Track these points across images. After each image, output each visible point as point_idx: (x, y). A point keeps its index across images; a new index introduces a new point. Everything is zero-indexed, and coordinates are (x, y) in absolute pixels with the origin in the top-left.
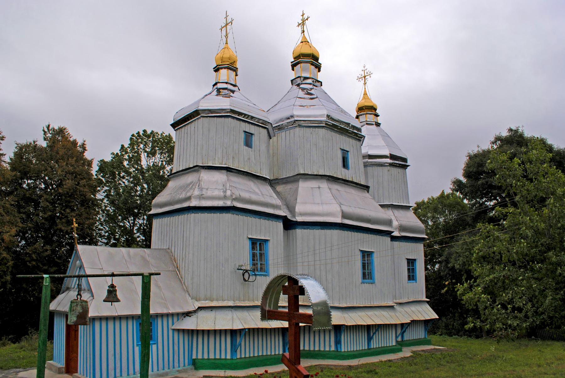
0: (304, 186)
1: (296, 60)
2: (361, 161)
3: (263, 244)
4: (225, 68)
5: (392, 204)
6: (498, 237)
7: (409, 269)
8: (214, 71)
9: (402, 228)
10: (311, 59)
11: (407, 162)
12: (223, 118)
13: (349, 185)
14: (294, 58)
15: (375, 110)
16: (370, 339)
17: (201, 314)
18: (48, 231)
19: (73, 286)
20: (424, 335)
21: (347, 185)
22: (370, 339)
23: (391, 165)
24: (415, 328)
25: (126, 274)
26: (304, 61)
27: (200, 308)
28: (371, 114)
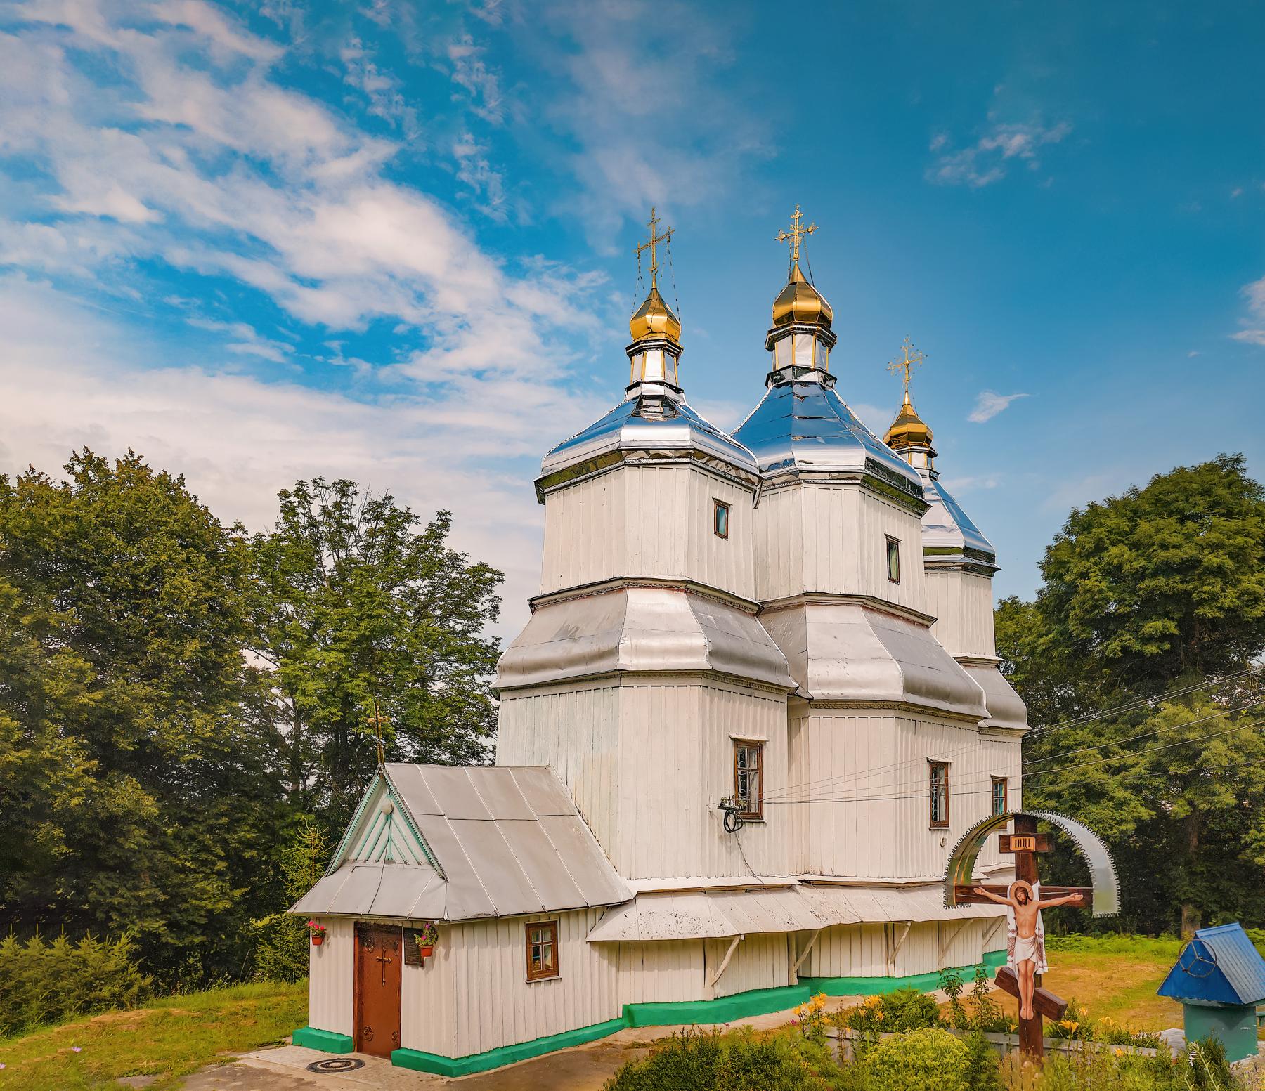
0: (815, 616)
1: (783, 327)
2: (920, 560)
4: (657, 348)
8: (628, 354)
15: (929, 441)
17: (640, 901)
19: (363, 856)
23: (966, 568)
25: (365, 827)
26: (802, 329)
27: (640, 894)
28: (921, 452)
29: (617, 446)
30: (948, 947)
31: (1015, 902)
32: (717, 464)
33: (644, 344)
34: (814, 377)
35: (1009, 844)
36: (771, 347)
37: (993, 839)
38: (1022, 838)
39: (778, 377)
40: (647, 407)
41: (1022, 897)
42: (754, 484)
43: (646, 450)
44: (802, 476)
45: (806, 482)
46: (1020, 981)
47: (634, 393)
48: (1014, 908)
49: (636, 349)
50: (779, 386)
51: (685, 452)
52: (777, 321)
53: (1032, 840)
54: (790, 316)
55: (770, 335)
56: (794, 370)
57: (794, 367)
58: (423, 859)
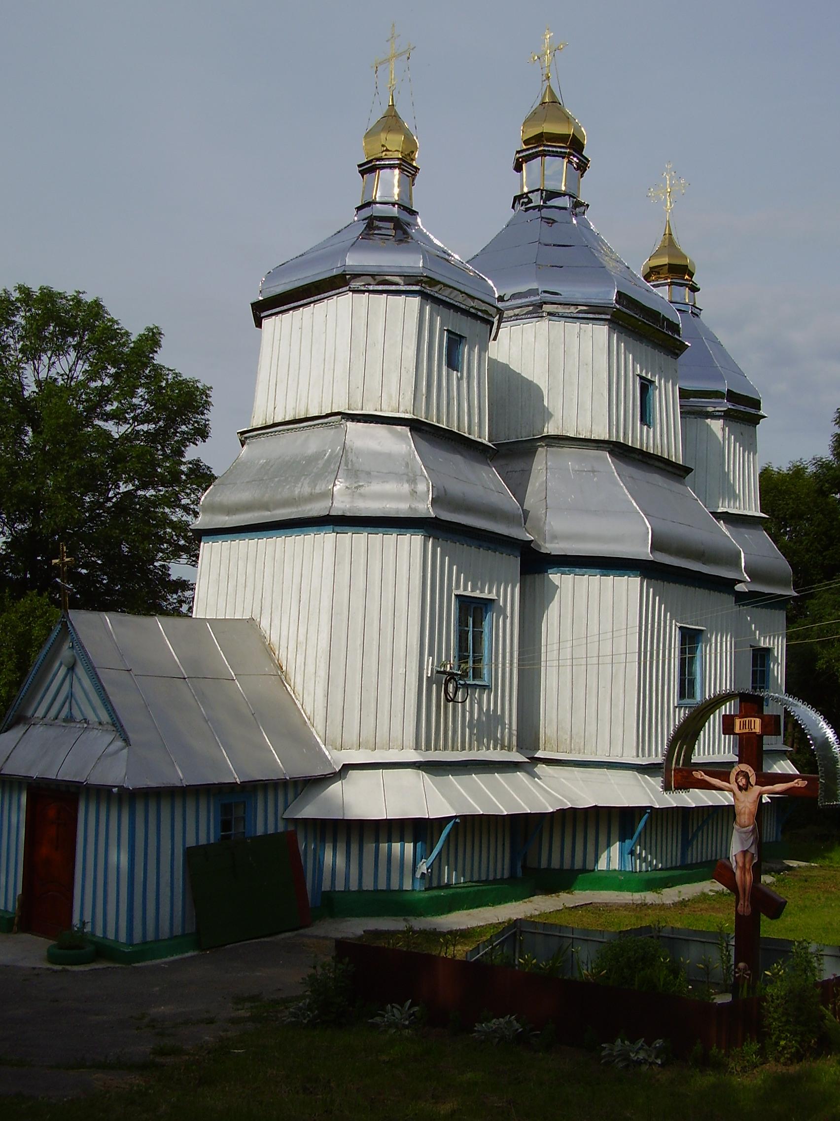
1: (531, 148)
3: (481, 610)
5: (727, 512)
6: (58, 517)
7: (754, 673)
8: (360, 172)
9: (755, 575)
10: (570, 148)
11: (758, 408)
12: (403, 297)
13: (652, 465)
14: (526, 142)
15: (691, 275)
16: (686, 844)
18: (105, 582)
19: (40, 713)
20: (507, 866)
21: (648, 464)
22: (686, 844)
24: (484, 841)
29: (340, 271)
30: (695, 835)
31: (734, 787)
32: (451, 293)
33: (378, 163)
34: (566, 202)
35: (733, 725)
36: (518, 168)
37: (715, 721)
38: (747, 719)
39: (526, 200)
40: (380, 228)
41: (742, 782)
42: (491, 315)
43: (373, 276)
44: (547, 308)
45: (550, 314)
46: (738, 873)
47: (366, 212)
48: (734, 794)
49: (368, 169)
50: (527, 210)
51: (414, 279)
52: (526, 142)
53: (758, 721)
54: (539, 139)
55: (518, 155)
56: (542, 193)
57: (542, 190)
58: (105, 717)
